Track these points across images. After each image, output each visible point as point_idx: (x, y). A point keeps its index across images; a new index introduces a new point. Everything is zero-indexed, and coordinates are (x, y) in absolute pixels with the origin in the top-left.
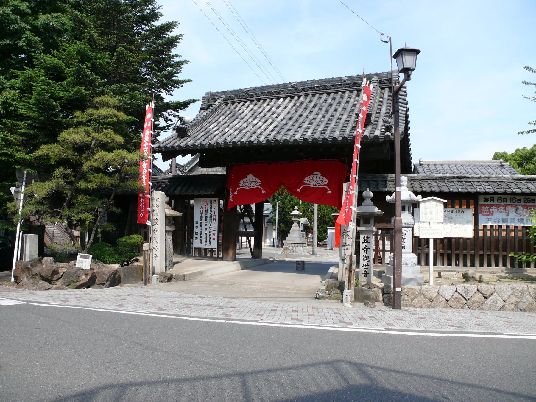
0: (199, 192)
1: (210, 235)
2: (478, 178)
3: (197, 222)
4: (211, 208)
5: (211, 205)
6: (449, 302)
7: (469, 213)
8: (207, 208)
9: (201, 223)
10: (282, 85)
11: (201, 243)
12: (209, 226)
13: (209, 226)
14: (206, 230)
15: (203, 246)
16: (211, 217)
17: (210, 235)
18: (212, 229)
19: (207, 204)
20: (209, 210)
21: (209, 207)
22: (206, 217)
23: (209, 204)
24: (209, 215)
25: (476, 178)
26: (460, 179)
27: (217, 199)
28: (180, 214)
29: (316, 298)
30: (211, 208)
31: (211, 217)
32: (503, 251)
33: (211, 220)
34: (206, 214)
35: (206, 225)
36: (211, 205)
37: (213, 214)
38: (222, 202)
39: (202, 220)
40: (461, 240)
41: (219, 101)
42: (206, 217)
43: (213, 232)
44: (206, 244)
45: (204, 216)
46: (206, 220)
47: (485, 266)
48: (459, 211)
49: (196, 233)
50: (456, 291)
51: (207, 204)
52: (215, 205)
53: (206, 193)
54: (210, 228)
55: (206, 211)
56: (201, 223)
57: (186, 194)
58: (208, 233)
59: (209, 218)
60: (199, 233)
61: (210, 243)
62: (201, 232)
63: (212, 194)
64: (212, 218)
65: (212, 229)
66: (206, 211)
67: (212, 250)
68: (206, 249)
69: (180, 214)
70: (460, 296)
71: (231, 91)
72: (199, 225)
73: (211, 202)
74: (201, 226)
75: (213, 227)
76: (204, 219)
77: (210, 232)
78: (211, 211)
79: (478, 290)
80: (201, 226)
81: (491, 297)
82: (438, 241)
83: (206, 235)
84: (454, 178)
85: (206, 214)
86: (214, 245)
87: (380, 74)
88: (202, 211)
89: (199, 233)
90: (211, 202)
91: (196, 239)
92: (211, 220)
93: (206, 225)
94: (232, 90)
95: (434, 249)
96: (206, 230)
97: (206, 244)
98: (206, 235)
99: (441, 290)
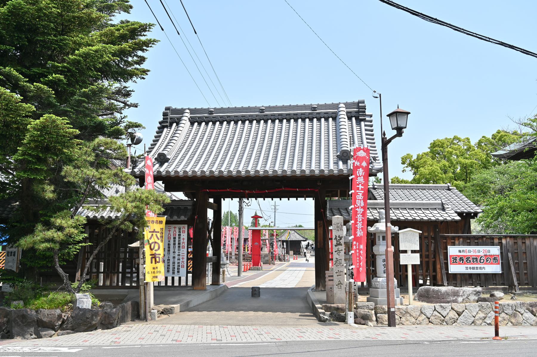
1: (178, 263)
4: (179, 235)
12: (177, 253)
13: (177, 253)
14: (174, 257)
16: (179, 244)
17: (178, 263)
18: (181, 257)
22: (174, 244)
24: (177, 242)
31: (179, 244)
33: (179, 247)
34: (175, 241)
35: (174, 252)
37: (182, 241)
39: (169, 247)
42: (174, 244)
43: (181, 260)
46: (174, 247)
50: (435, 310)
59: (177, 245)
64: (181, 245)
65: (181, 257)
78: (179, 238)
79: (452, 308)
83: (174, 263)
85: (175, 241)
92: (179, 247)
93: (174, 252)
96: (174, 257)
98: (174, 263)
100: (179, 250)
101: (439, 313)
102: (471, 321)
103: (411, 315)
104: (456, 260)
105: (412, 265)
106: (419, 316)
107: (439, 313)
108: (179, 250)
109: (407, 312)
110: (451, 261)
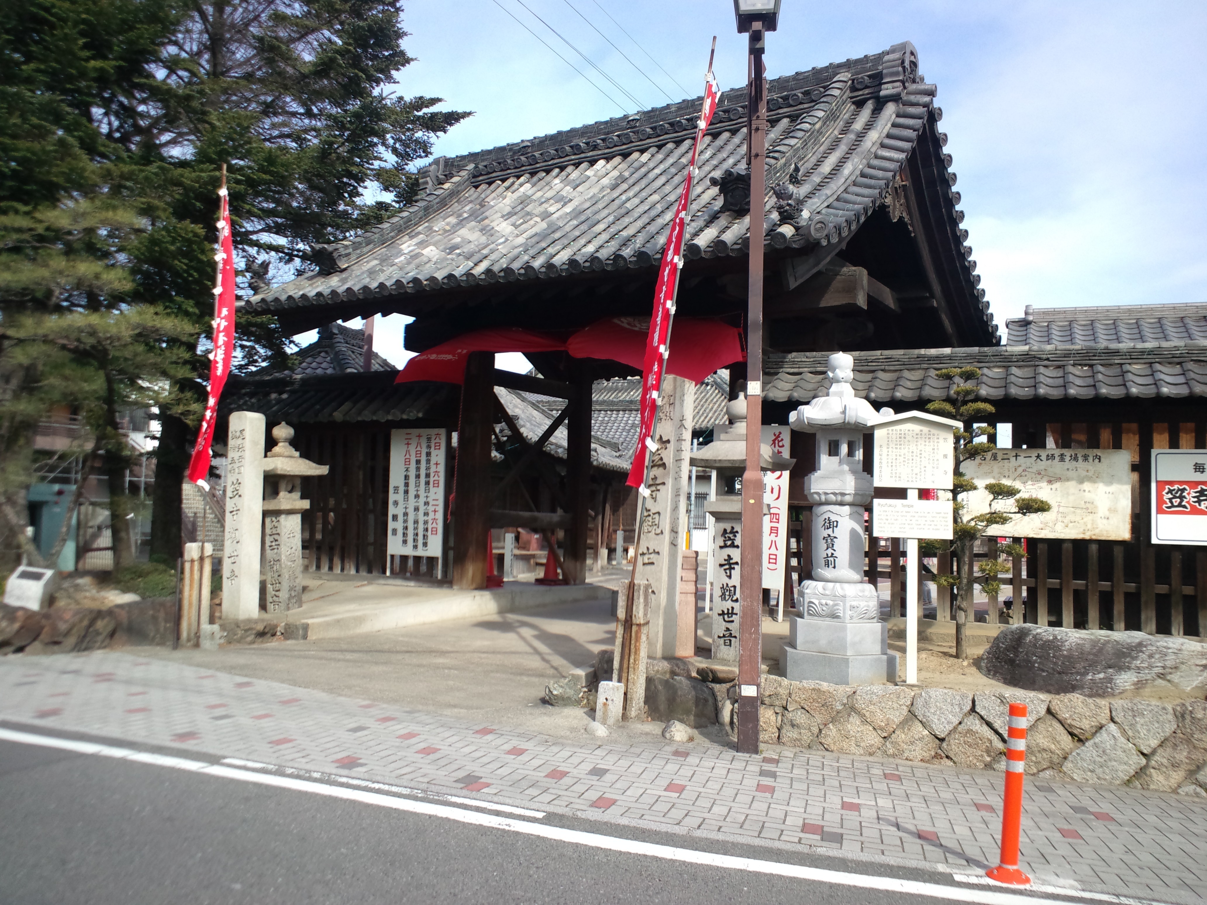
0: (403, 412)
1: (426, 522)
2: (1150, 352)
3: (396, 489)
4: (428, 454)
5: (429, 447)
6: (944, 745)
7: (1122, 460)
8: (418, 453)
9: (406, 492)
10: (606, 123)
11: (405, 542)
12: (422, 500)
13: (422, 500)
14: (417, 509)
15: (408, 551)
16: (428, 475)
17: (426, 522)
18: (431, 508)
19: (419, 444)
20: (423, 459)
21: (424, 451)
22: (418, 476)
23: (424, 445)
24: (423, 472)
25: (1143, 352)
26: (1088, 358)
27: (443, 432)
28: (323, 470)
29: (545, 702)
30: (428, 454)
31: (428, 475)
32: (1075, 579)
33: (427, 483)
34: (418, 469)
35: (417, 496)
36: (429, 447)
37: (433, 468)
38: (455, 436)
39: (407, 485)
40: (1094, 548)
41: (456, 179)
42: (418, 476)
43: (431, 515)
44: (415, 547)
45: (412, 473)
46: (417, 485)
47: (1174, 631)
48: (1062, 458)
49: (395, 518)
50: (973, 709)
51: (419, 444)
52: (438, 447)
53: (405, 417)
54: (427, 503)
55: (418, 462)
56: (406, 492)
57: (360, 419)
58: (421, 518)
59: (423, 479)
60: (401, 518)
61: (425, 544)
62: (406, 514)
63: (418, 419)
64: (432, 479)
65: (431, 508)
66: (418, 462)
67: (432, 560)
68: (417, 559)
69: (323, 470)
70: (985, 728)
71: (489, 152)
72: (400, 497)
73: (429, 439)
74: (406, 499)
75: (431, 503)
76: (412, 481)
77: (426, 514)
78: (428, 461)
79: (1049, 711)
80: (406, 499)
81: (1097, 739)
82: (1041, 548)
83: (416, 522)
84: (1067, 355)
85: (418, 469)
86: (435, 548)
87: (857, 61)
88: (407, 462)
89: (401, 518)
90: (429, 439)
91: (395, 531)
92: (427, 483)
93: (417, 496)
94: (490, 147)
95: (904, 568)
96: (417, 509)
97: (415, 547)
98: (416, 522)
99: (919, 703)
100: (427, 490)
101: (989, 724)
102: (1125, 770)
103: (865, 721)
104: (1182, 498)
105: (920, 540)
106: (903, 724)
107: (989, 724)
108: (427, 490)
109: (852, 709)
110: (1160, 501)
